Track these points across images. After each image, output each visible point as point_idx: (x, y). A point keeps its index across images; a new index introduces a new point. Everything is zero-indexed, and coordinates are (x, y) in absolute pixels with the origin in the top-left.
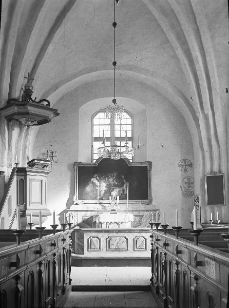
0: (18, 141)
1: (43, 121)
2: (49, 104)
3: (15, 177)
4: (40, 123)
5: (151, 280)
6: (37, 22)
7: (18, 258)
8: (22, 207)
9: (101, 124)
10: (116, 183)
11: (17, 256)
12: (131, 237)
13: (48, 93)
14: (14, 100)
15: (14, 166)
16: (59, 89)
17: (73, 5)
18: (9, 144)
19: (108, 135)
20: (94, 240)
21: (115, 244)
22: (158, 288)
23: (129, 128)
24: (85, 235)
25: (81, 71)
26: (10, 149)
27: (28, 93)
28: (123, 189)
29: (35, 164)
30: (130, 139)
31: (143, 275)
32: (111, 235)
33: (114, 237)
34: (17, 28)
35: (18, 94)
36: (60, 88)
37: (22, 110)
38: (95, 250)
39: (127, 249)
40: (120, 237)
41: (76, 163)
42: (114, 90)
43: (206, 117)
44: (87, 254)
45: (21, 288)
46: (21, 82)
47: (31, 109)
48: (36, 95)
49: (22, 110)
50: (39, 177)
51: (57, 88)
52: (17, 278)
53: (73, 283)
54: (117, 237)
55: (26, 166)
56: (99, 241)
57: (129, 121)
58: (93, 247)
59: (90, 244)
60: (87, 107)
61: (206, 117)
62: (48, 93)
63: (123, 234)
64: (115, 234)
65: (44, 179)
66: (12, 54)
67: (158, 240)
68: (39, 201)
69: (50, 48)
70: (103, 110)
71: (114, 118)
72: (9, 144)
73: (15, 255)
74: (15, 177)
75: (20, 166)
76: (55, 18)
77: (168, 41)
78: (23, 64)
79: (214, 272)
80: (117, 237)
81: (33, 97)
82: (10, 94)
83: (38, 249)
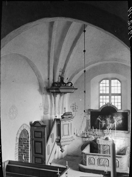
0: (59, 101)
3: (56, 123)
6: (64, 42)
8: (59, 138)
10: (110, 121)
13: (72, 77)
16: (79, 73)
17: (80, 36)
18: (55, 103)
20: (92, 159)
21: (102, 162)
23: (120, 88)
24: (87, 156)
25: (89, 63)
26: (55, 106)
27: (62, 79)
28: (114, 125)
29: (64, 117)
30: (120, 95)
32: (100, 157)
33: (102, 158)
34: (53, 51)
35: (57, 80)
36: (80, 72)
37: (57, 91)
38: (92, 164)
39: (109, 165)
40: (105, 159)
41: (90, 110)
44: (88, 167)
46: (58, 73)
48: (65, 81)
49: (57, 91)
50: (67, 122)
51: (78, 72)
54: (103, 159)
55: (60, 118)
56: (94, 159)
57: (119, 85)
58: (91, 162)
59: (90, 160)
64: (102, 157)
66: (53, 62)
68: (67, 134)
69: (72, 56)
71: (103, 94)
72: (55, 103)
74: (56, 123)
75: (57, 118)
76: (72, 42)
78: (58, 67)
80: (103, 159)
82: (54, 80)
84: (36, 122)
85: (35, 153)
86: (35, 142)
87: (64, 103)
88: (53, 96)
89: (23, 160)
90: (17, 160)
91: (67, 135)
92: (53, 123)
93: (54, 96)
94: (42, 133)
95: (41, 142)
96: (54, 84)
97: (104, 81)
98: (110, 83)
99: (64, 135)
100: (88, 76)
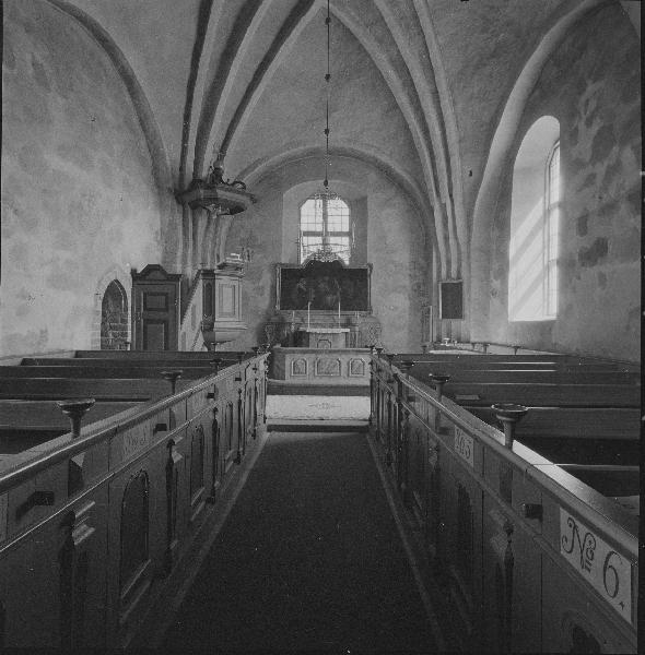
1: (236, 209)
2: (244, 188)
4: (232, 212)
5: (370, 420)
7: (172, 416)
9: (310, 214)
11: (171, 411)
12: (344, 359)
14: (201, 181)
15: (200, 267)
19: (319, 228)
22: (378, 432)
31: (357, 409)
32: (320, 356)
35: (205, 173)
42: (320, 167)
43: (443, 206)
44: (289, 380)
45: (177, 457)
46: (209, 157)
47: (220, 193)
48: (228, 175)
52: (171, 443)
53: (268, 422)
58: (297, 371)
60: (289, 194)
61: (443, 206)
62: (244, 172)
63: (335, 355)
65: (236, 283)
67: (379, 370)
70: (312, 197)
72: (194, 239)
73: (168, 410)
77: (396, 106)
79: (472, 452)
81: (224, 178)
82: (195, 174)
83: (212, 391)
84: (150, 269)
85: (165, 322)
86: (147, 321)
87: (215, 239)
88: (190, 212)
89: (127, 343)
90: (97, 347)
91: (229, 314)
92: (195, 282)
93: (193, 214)
94: (167, 299)
95: (165, 322)
96: (196, 182)
97: (310, 203)
98: (325, 206)
99: (222, 315)
100: (276, 181)
